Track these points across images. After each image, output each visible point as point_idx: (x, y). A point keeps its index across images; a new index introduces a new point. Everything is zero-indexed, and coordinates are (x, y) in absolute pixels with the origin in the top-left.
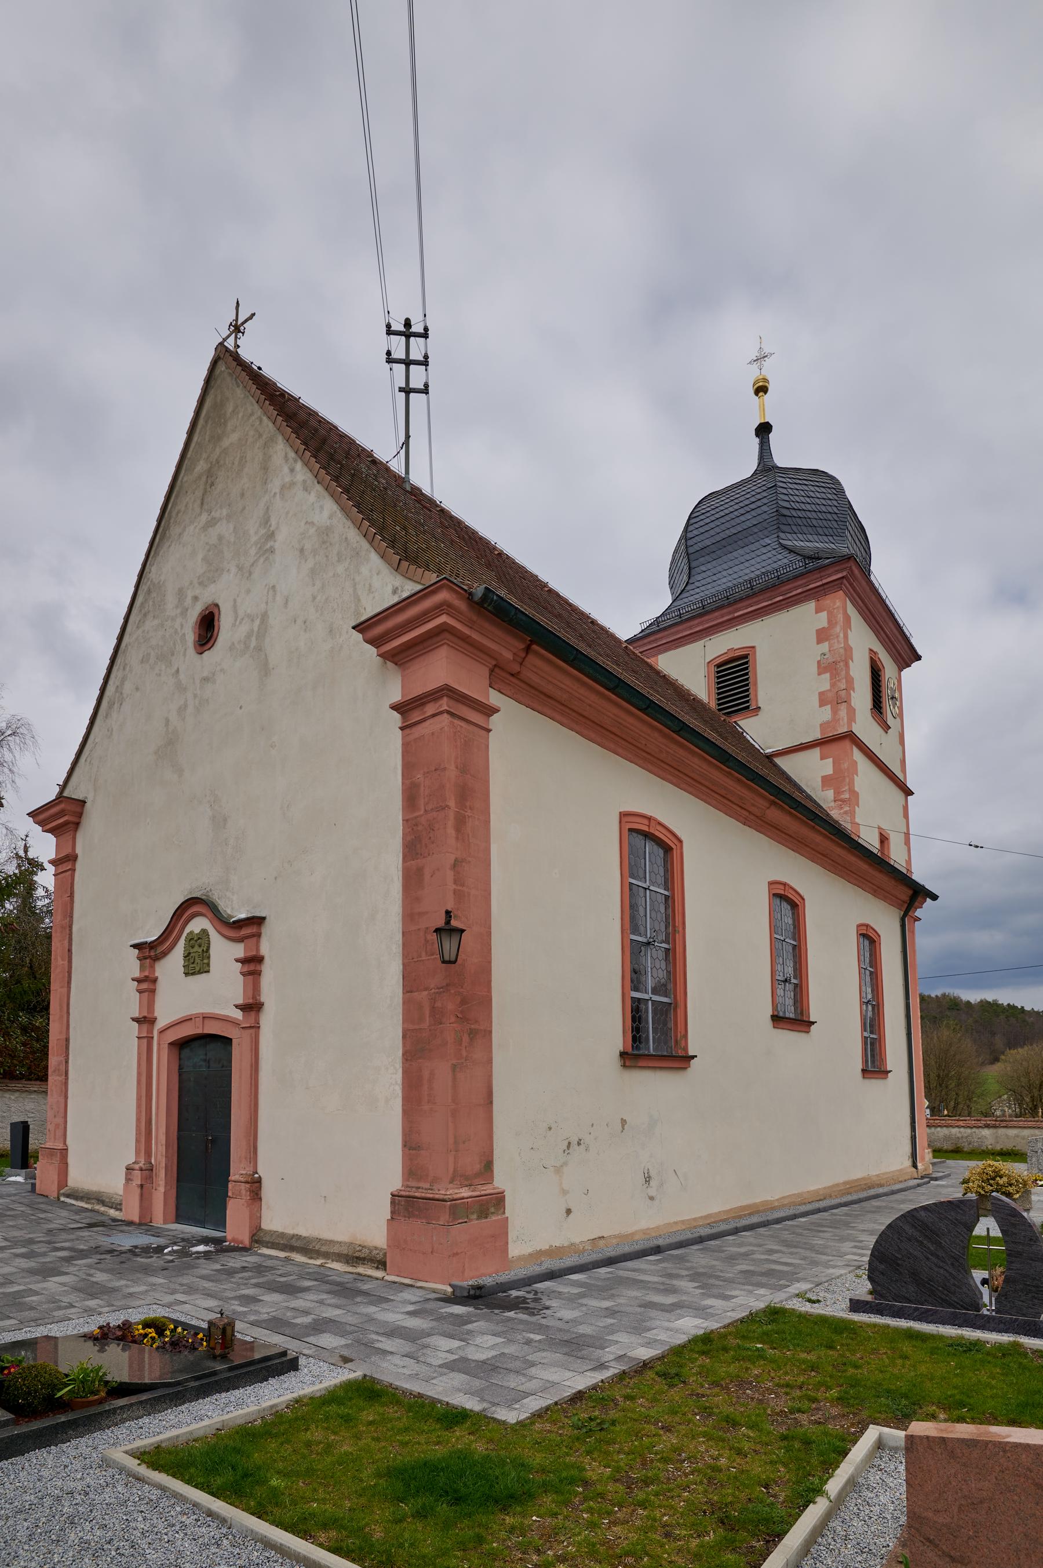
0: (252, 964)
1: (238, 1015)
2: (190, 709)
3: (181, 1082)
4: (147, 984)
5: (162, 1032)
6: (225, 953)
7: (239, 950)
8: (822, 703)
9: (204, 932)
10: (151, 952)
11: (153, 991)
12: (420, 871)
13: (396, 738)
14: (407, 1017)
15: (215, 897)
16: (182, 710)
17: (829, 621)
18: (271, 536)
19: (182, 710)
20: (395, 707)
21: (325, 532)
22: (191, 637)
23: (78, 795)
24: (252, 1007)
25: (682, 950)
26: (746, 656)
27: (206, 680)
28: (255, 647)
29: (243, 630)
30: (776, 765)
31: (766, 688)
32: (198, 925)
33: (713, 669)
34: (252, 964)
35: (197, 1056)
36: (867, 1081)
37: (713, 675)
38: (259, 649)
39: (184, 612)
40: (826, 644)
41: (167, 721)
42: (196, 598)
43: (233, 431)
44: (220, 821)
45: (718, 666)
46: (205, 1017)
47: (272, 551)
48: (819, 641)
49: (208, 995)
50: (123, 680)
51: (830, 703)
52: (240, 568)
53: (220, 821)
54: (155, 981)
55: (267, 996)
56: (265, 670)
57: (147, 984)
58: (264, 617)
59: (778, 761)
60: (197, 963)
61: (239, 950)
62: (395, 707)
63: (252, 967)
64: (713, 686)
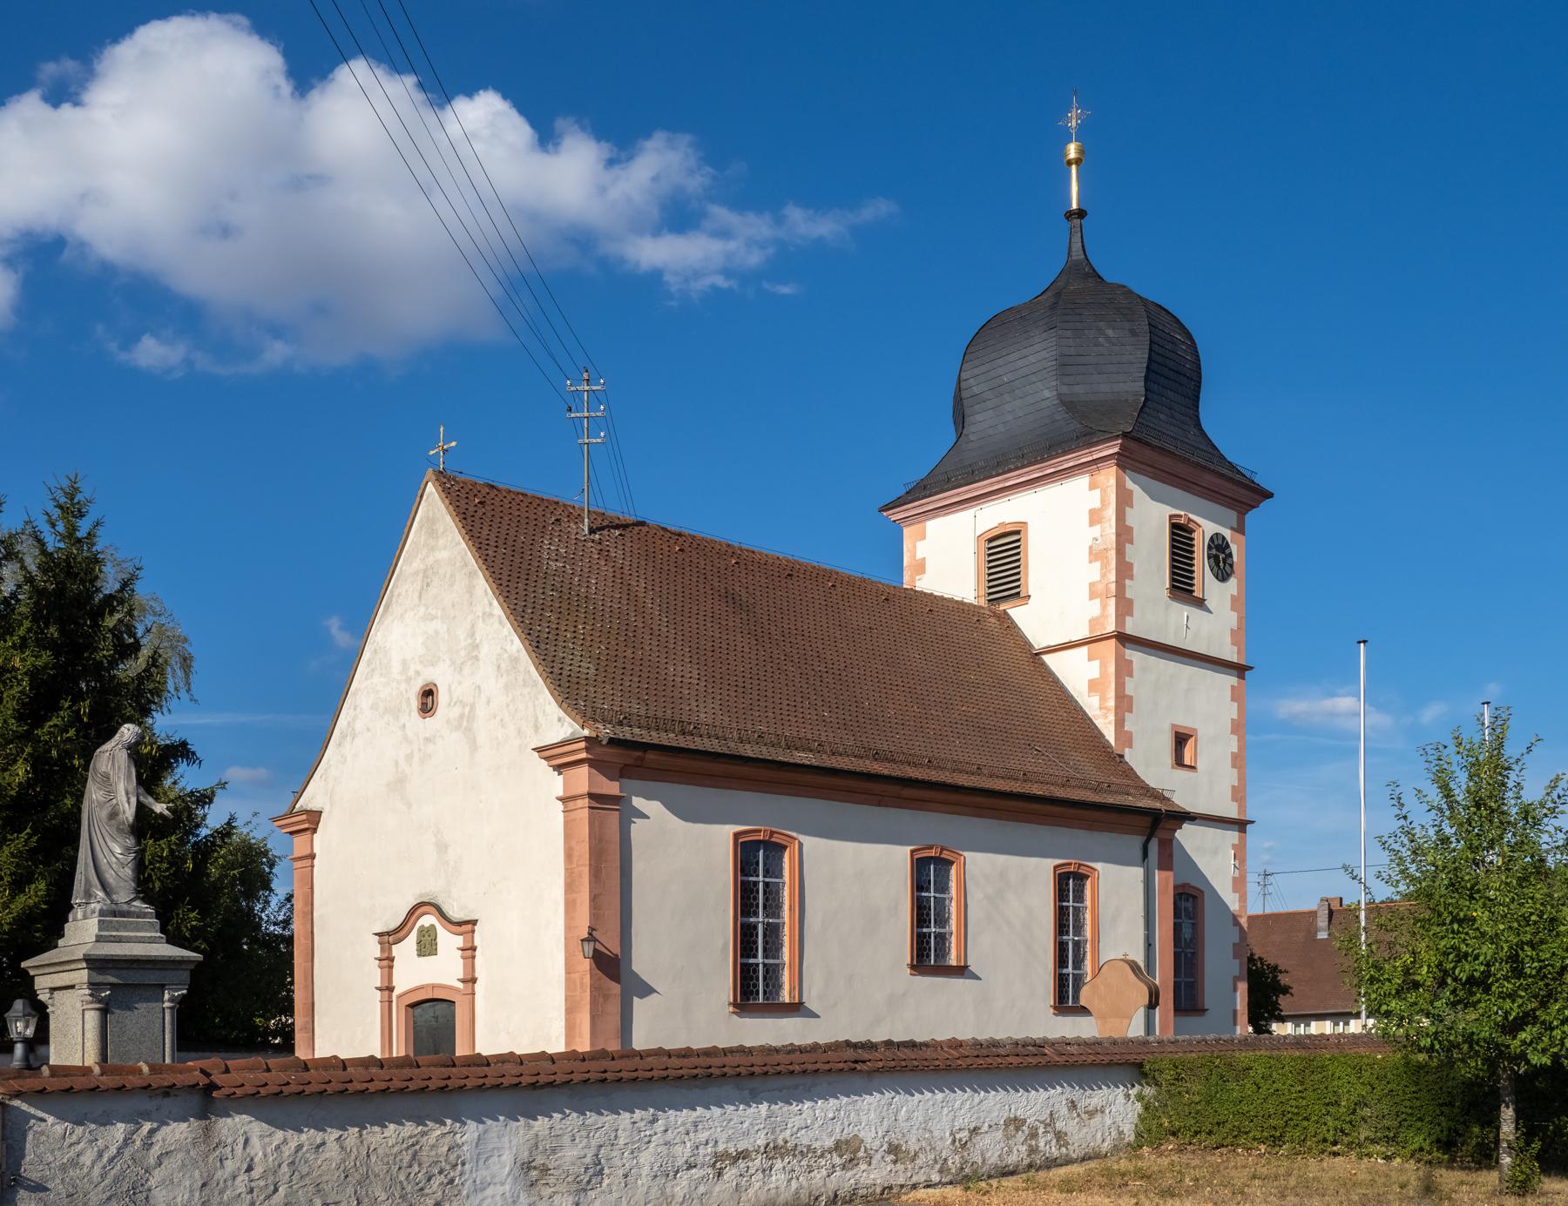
0: (469, 951)
1: (460, 985)
2: (416, 759)
3: (415, 1033)
4: (387, 961)
5: (399, 997)
6: (449, 942)
7: (459, 941)
8: (1092, 596)
9: (433, 926)
10: (388, 939)
11: (391, 967)
12: (574, 901)
13: (561, 817)
14: (568, 988)
15: (440, 901)
16: (409, 757)
17: (1103, 501)
18: (476, 647)
19: (409, 757)
20: (560, 799)
21: (515, 660)
22: (415, 704)
23: (314, 805)
24: (471, 980)
25: (467, 1023)
26: (1018, 532)
27: (427, 740)
28: (466, 724)
29: (456, 711)
30: (1043, 664)
31: (1038, 569)
32: (428, 920)
33: (985, 545)
34: (469, 951)
35: (428, 1012)
36: (1060, 1018)
37: (983, 551)
38: (469, 729)
39: (408, 680)
40: (1098, 527)
41: (397, 763)
42: (418, 673)
43: (445, 548)
44: (442, 848)
45: (990, 540)
46: (434, 986)
47: (476, 658)
48: (1092, 523)
49: (439, 970)
50: (355, 718)
51: (1100, 596)
52: (453, 663)
53: (442, 848)
54: (392, 960)
55: (480, 972)
56: (474, 747)
57: (387, 961)
58: (472, 706)
59: (1046, 658)
60: (427, 946)
61: (459, 941)
62: (560, 799)
63: (469, 953)
64: (984, 565)
